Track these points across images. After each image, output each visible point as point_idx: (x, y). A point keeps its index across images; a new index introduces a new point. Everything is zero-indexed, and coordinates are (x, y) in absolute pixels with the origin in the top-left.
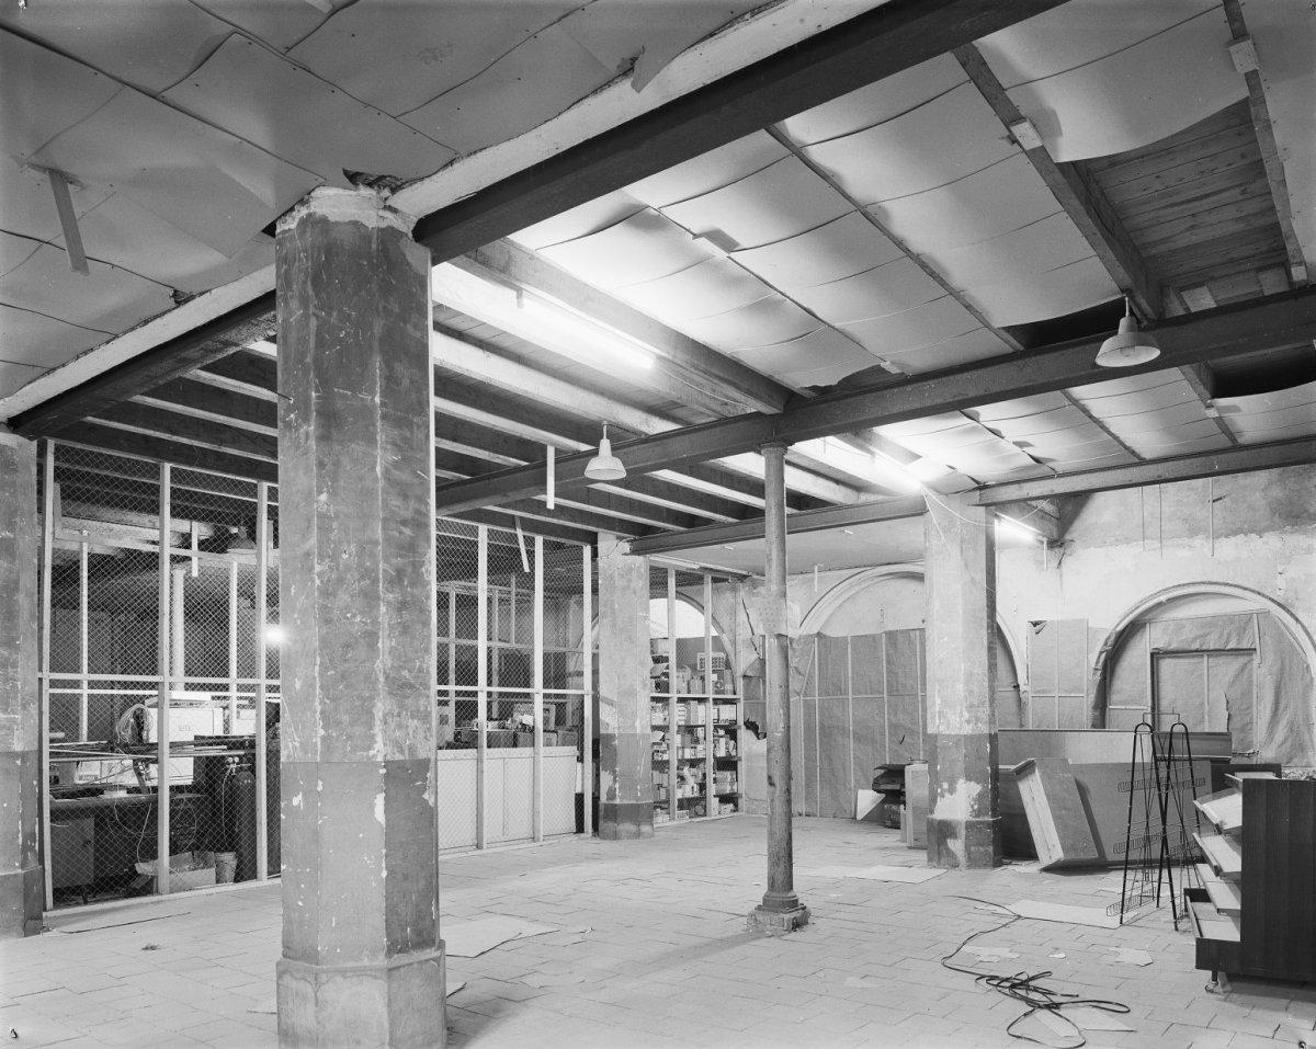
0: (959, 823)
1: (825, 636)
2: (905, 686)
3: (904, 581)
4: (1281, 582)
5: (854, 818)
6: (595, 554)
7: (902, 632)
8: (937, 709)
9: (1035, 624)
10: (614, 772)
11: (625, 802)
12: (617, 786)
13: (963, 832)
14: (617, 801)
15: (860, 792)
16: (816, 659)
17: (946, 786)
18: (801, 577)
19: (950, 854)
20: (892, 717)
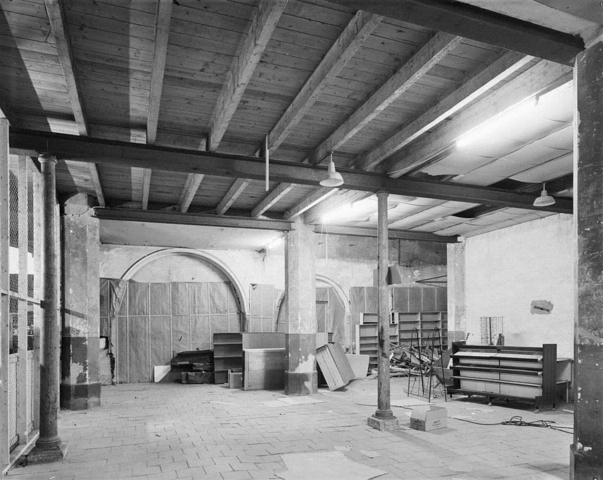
0: (310, 374)
1: (134, 282)
2: (183, 311)
3: (183, 257)
4: (339, 277)
5: (153, 381)
6: (62, 212)
7: (181, 283)
8: (300, 322)
9: (253, 285)
10: (85, 363)
11: (92, 383)
12: (87, 372)
13: (312, 378)
14: (87, 383)
15: (156, 368)
16: (128, 291)
17: (303, 357)
18: (125, 246)
19: (306, 388)
20: (174, 327)
